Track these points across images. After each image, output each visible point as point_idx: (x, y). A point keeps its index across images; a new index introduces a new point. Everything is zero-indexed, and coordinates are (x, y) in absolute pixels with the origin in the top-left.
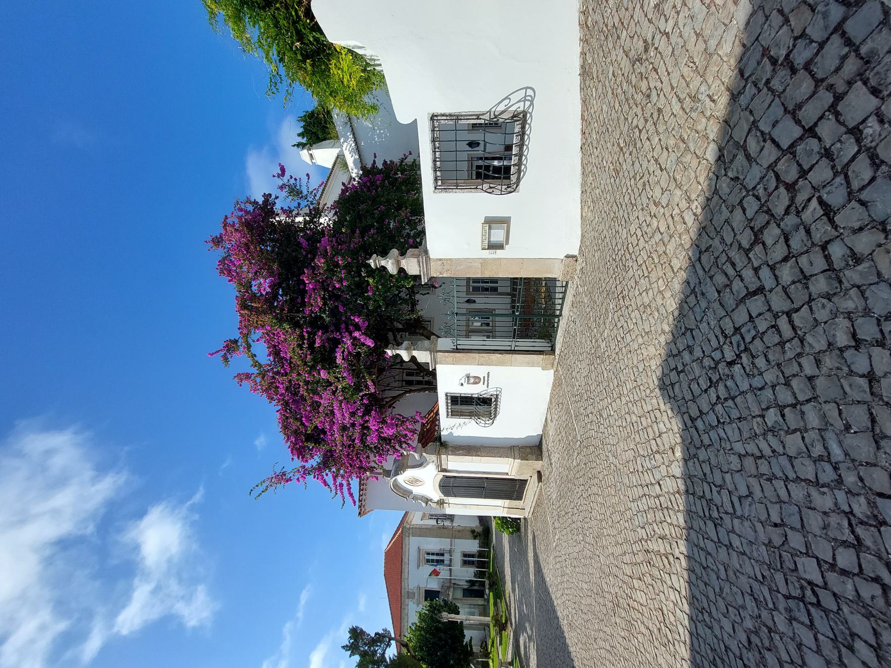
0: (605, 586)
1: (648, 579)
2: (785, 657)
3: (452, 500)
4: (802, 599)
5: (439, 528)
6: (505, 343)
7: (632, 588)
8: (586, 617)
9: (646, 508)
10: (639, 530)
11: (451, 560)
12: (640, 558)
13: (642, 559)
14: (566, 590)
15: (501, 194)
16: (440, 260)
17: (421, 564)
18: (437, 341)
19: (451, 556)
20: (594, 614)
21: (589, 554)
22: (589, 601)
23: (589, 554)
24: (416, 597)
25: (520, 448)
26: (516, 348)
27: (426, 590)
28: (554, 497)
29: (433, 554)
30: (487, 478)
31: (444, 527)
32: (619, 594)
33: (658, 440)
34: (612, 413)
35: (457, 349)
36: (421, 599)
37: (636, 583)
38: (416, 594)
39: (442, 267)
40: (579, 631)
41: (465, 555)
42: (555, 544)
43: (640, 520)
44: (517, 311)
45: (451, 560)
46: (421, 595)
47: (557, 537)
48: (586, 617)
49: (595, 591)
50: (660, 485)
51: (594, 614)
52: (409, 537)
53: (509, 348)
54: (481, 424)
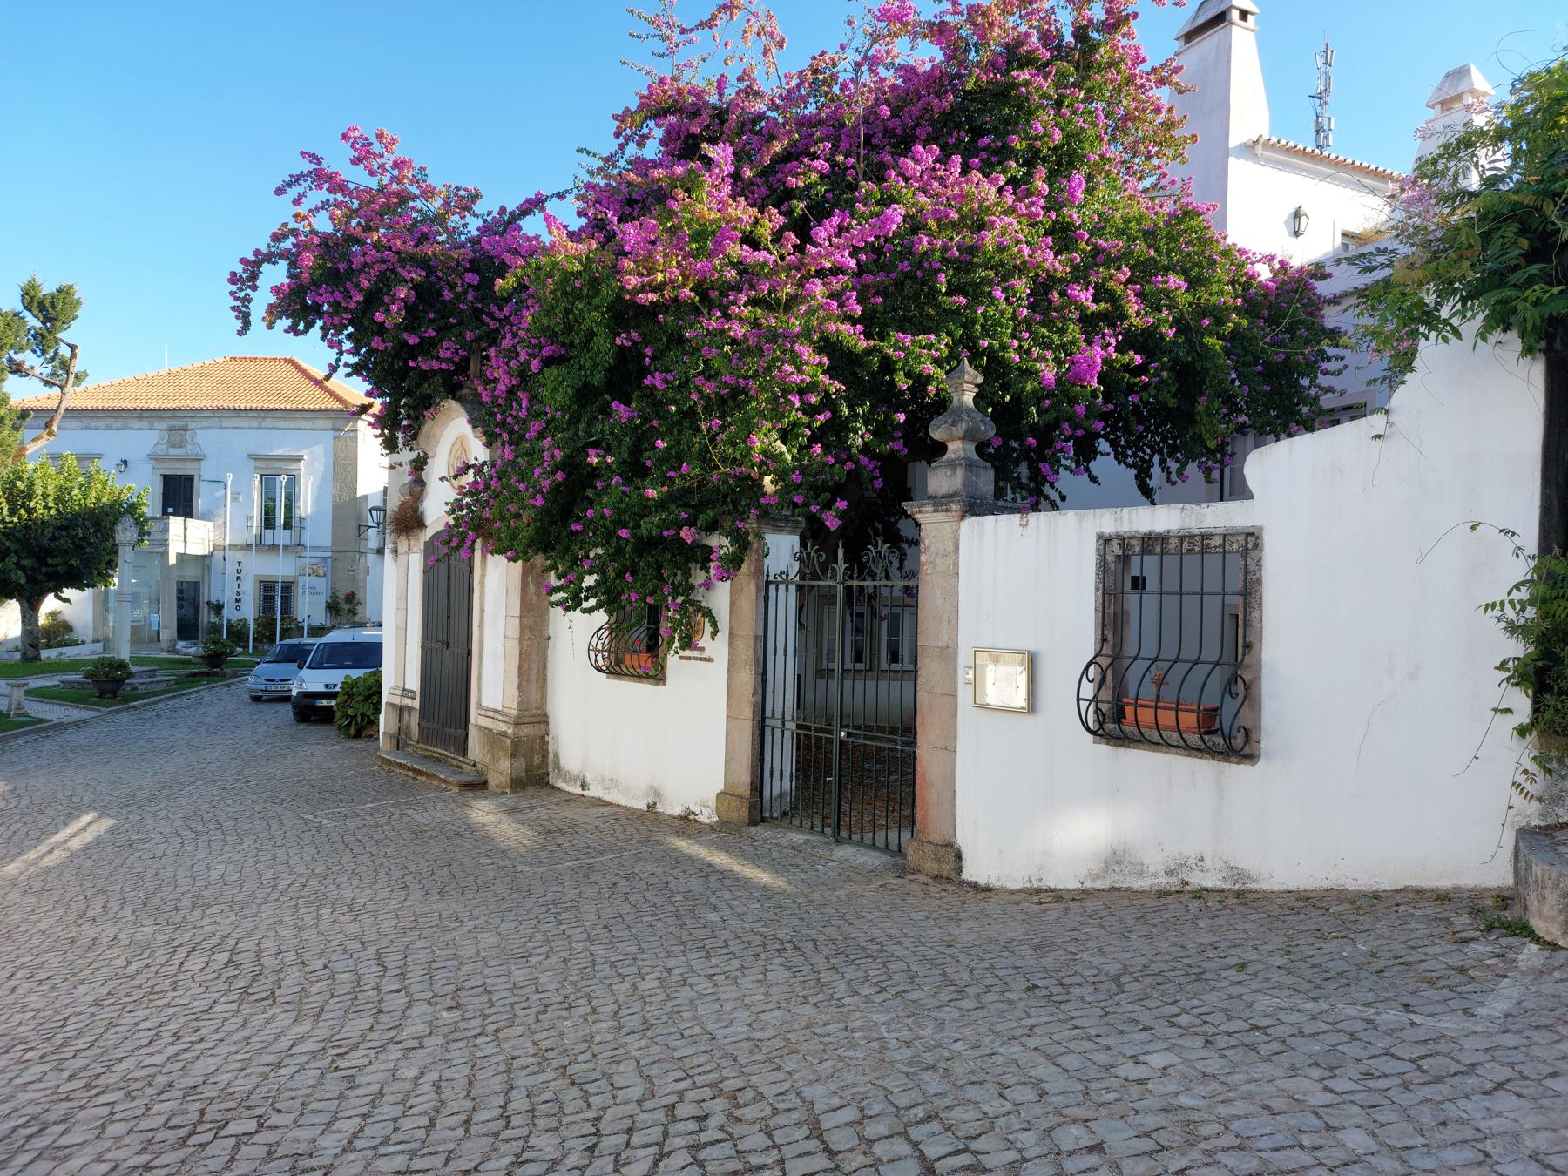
0: (215, 909)
1: (230, 972)
2: (117, 1108)
3: (416, 562)
4: (200, 1122)
5: (359, 516)
6: (783, 700)
7: (213, 950)
8: (149, 874)
9: (360, 971)
10: (323, 961)
11: (274, 547)
12: (270, 962)
13: (266, 965)
14: (205, 838)
15: (1078, 699)
16: (957, 549)
17: (259, 464)
18: (792, 532)
19: (286, 547)
20: (159, 888)
21: (282, 884)
22: (184, 883)
23: (282, 884)
24: (173, 451)
25: (543, 738)
26: (768, 731)
27: (190, 480)
28: (419, 818)
29: (289, 498)
30: (469, 653)
31: (361, 528)
32: (199, 931)
33: (482, 989)
34: (562, 927)
35: (768, 583)
36: (166, 465)
37: (224, 957)
38: (181, 452)
39: (941, 551)
40: (118, 861)
41: (287, 587)
42: (310, 817)
43: (340, 964)
44: (849, 735)
45: (274, 547)
46: (179, 465)
47: (325, 822)
48: (149, 874)
49: (205, 893)
50: (398, 991)
51: (159, 888)
52: (333, 430)
53: (768, 713)
54: (595, 639)
